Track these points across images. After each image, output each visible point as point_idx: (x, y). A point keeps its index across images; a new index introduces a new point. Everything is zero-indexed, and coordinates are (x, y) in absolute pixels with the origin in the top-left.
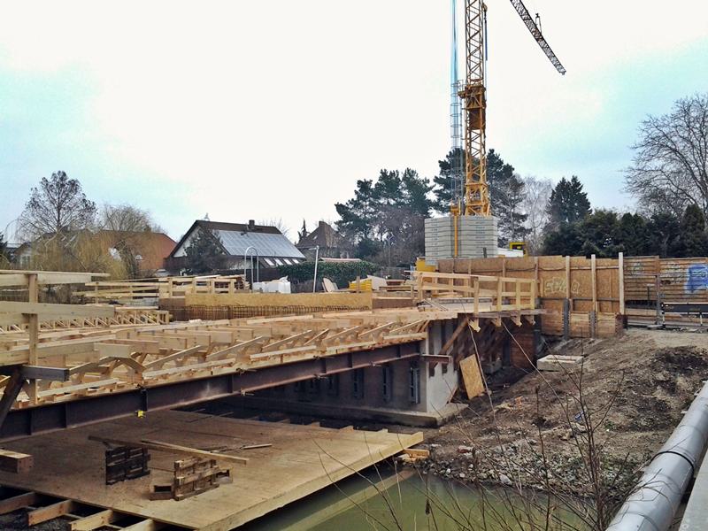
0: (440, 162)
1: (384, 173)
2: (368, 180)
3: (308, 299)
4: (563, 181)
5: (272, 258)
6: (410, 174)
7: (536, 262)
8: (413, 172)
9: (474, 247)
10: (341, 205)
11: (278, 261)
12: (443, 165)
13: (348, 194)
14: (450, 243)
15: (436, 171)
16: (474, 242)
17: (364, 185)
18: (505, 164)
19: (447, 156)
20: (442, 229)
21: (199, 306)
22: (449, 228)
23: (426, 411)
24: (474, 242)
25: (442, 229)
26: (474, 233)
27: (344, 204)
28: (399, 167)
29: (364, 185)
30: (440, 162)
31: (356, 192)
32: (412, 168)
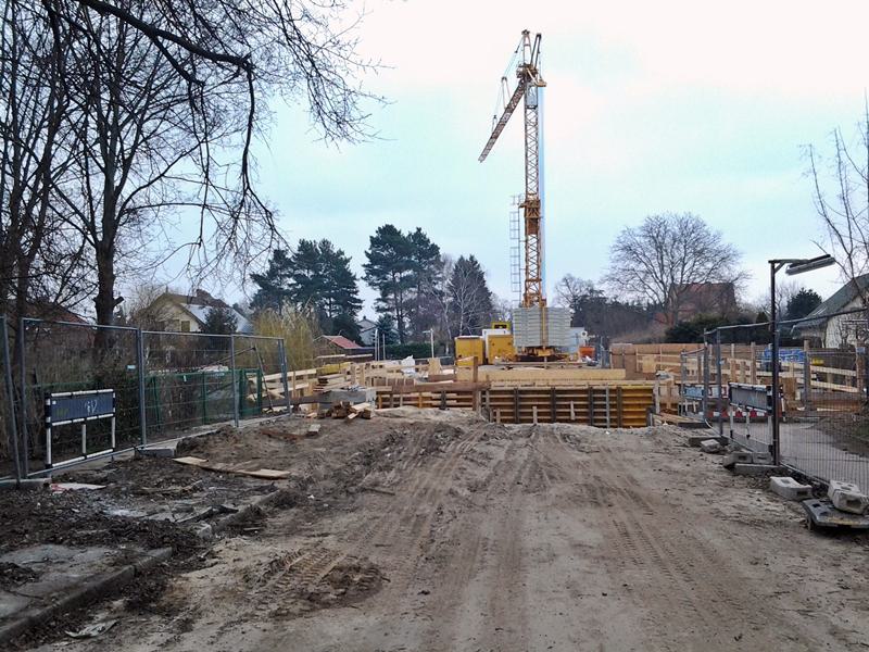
4: (462, 258)
6: (325, 243)
12: (374, 241)
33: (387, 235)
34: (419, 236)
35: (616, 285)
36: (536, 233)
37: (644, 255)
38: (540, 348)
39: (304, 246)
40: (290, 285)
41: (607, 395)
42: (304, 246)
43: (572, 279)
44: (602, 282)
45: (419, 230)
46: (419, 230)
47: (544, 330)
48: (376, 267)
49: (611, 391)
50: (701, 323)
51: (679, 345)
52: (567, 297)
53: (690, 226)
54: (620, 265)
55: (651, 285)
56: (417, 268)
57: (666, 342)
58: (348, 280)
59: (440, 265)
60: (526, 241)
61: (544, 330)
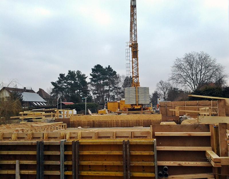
0: (92, 69)
1: (70, 71)
2: (63, 74)
3: (132, 117)
4: (127, 77)
5: (36, 102)
6: (79, 72)
7: (197, 103)
8: (79, 71)
9: (143, 98)
10: (53, 82)
11: (41, 103)
12: (93, 70)
13: (56, 80)
14: (135, 96)
15: (91, 72)
16: (143, 96)
17: (62, 76)
18: (114, 70)
19: (94, 67)
20: (132, 91)
21: (78, 121)
22: (134, 91)
23: (221, 174)
24: (143, 96)
25: (132, 91)
26: (143, 93)
27: (55, 82)
28: (75, 69)
29: (62, 76)
30: (92, 69)
31: (59, 78)
32: (80, 70)
33: (98, 69)
34: (109, 68)
35: (175, 81)
36: (137, 58)
37: (185, 69)
38: (136, 105)
39: (70, 72)
40: (65, 86)
41: (61, 153)
42: (70, 72)
43: (163, 82)
44: (169, 80)
45: (109, 66)
46: (109, 66)
47: (137, 97)
48: (94, 79)
49: (67, 147)
50: (207, 91)
51: (195, 101)
52: (161, 88)
53: (203, 57)
54: (176, 73)
55: (189, 81)
56: (109, 79)
57: (189, 100)
58: (85, 84)
59: (117, 78)
60: (132, 61)
61: (137, 97)
